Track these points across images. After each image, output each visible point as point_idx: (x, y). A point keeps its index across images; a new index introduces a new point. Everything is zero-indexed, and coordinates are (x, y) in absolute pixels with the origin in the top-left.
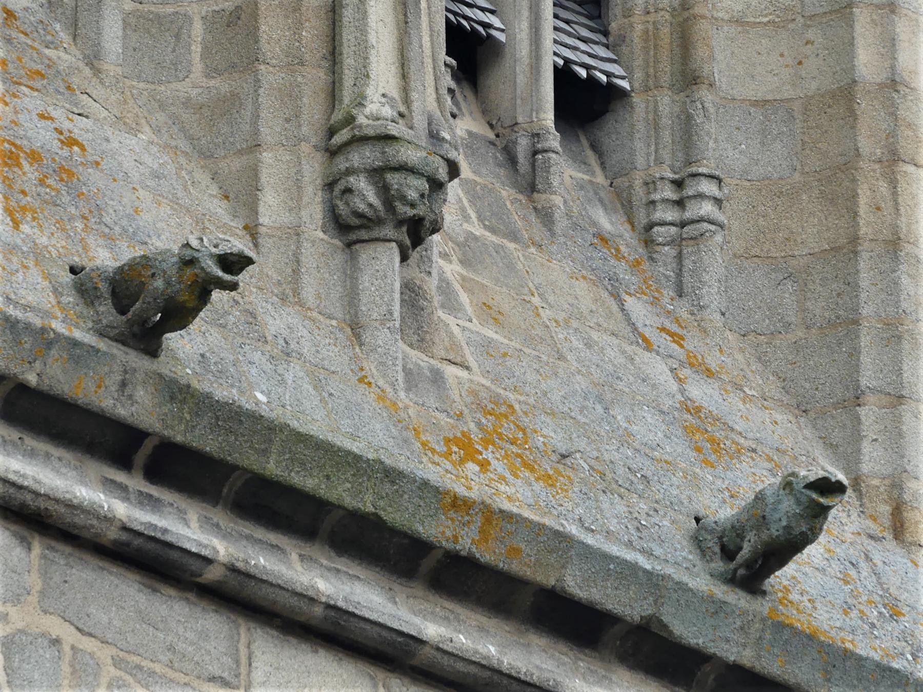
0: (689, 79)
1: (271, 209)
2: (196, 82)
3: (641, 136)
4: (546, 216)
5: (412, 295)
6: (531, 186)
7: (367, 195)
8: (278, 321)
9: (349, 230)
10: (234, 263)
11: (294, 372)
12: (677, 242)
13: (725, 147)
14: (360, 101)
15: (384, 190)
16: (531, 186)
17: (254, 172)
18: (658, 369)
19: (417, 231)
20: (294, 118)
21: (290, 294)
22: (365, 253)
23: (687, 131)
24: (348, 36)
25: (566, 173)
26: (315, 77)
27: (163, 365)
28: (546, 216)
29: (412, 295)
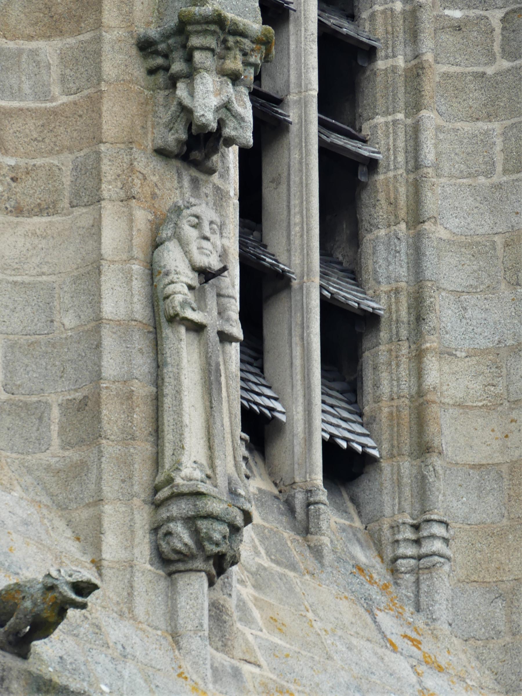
0: (423, 449)
1: (112, 548)
2: (55, 453)
3: (388, 491)
4: (317, 552)
5: (217, 613)
6: (306, 529)
7: (183, 537)
8: (117, 631)
9: (170, 563)
10: (84, 589)
11: (129, 670)
12: (415, 571)
13: (451, 499)
14: (177, 467)
15: (196, 533)
16: (306, 529)
17: (98, 520)
18: (402, 666)
19: (220, 564)
20: (128, 479)
21: (126, 611)
22: (182, 580)
23: (422, 488)
24: (168, 419)
25: (333, 520)
26: (143, 448)
27: (32, 665)
28: (317, 552)
29: (217, 613)
